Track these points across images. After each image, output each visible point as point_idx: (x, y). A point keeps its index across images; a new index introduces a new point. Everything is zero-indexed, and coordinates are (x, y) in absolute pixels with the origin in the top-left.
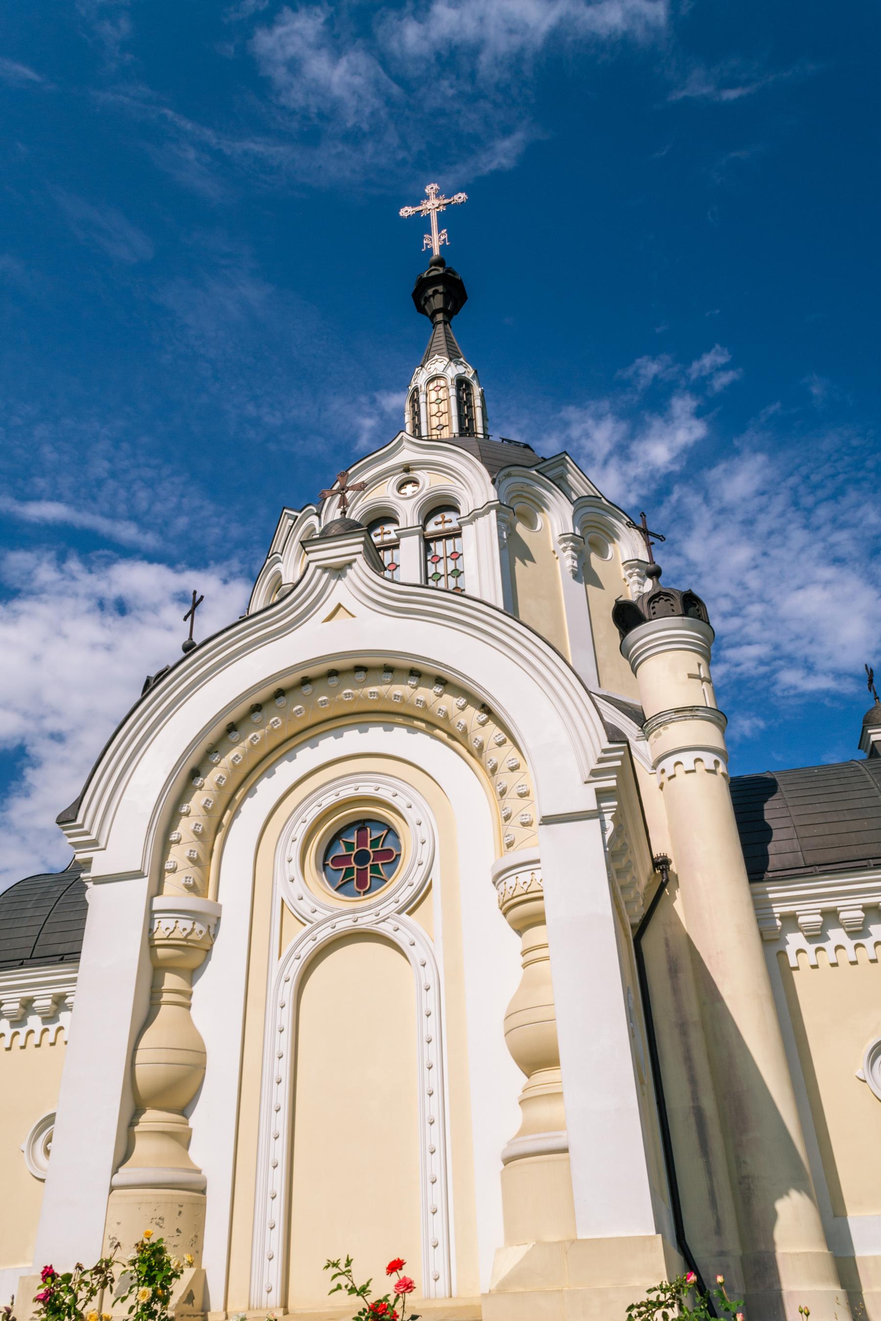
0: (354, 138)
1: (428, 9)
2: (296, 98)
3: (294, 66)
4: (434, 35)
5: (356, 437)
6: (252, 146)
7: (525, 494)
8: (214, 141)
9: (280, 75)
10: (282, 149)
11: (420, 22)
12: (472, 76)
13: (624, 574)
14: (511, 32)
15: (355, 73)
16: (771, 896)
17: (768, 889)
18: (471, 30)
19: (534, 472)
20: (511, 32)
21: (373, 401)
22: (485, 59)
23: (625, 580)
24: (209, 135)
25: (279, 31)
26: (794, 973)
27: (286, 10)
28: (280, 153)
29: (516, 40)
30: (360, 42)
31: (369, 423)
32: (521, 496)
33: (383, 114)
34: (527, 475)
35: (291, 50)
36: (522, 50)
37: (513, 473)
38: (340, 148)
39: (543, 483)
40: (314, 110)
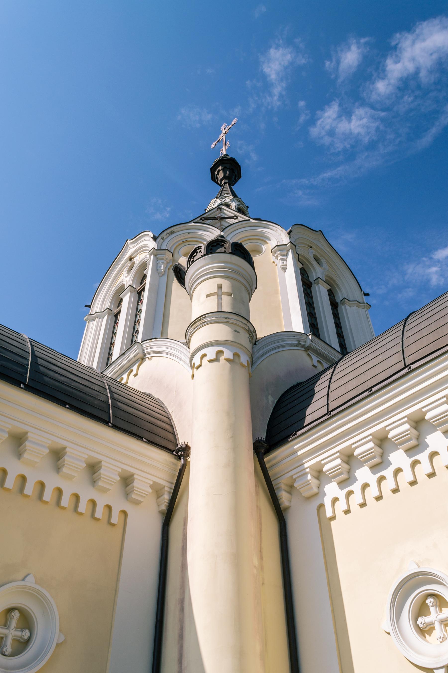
0: (372, 146)
1: (384, 71)
2: (339, 146)
3: (331, 133)
4: (392, 81)
5: (428, 281)
6: (325, 175)
7: (188, 240)
8: (307, 182)
9: (327, 140)
10: (339, 169)
11: (383, 79)
12: (419, 87)
13: (272, 258)
14: (431, 54)
15: (361, 119)
16: (299, 453)
17: (295, 447)
18: (411, 67)
19: (193, 224)
20: (431, 54)
21: (431, 258)
22: (423, 74)
23: (274, 262)
24: (305, 181)
25: (319, 122)
26: (333, 523)
27: (319, 112)
28: (340, 171)
29: (435, 56)
30: (357, 104)
31: (434, 269)
32: (187, 241)
33: (382, 127)
34: (189, 227)
35: (327, 127)
36: (440, 58)
37: (175, 230)
38: (366, 154)
39: (203, 228)
40: (348, 146)
